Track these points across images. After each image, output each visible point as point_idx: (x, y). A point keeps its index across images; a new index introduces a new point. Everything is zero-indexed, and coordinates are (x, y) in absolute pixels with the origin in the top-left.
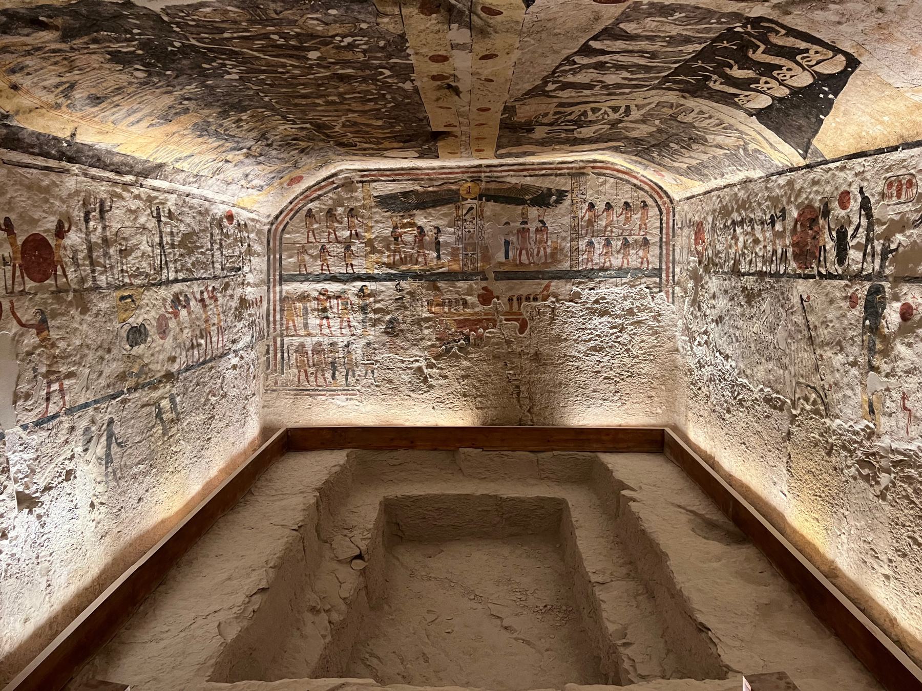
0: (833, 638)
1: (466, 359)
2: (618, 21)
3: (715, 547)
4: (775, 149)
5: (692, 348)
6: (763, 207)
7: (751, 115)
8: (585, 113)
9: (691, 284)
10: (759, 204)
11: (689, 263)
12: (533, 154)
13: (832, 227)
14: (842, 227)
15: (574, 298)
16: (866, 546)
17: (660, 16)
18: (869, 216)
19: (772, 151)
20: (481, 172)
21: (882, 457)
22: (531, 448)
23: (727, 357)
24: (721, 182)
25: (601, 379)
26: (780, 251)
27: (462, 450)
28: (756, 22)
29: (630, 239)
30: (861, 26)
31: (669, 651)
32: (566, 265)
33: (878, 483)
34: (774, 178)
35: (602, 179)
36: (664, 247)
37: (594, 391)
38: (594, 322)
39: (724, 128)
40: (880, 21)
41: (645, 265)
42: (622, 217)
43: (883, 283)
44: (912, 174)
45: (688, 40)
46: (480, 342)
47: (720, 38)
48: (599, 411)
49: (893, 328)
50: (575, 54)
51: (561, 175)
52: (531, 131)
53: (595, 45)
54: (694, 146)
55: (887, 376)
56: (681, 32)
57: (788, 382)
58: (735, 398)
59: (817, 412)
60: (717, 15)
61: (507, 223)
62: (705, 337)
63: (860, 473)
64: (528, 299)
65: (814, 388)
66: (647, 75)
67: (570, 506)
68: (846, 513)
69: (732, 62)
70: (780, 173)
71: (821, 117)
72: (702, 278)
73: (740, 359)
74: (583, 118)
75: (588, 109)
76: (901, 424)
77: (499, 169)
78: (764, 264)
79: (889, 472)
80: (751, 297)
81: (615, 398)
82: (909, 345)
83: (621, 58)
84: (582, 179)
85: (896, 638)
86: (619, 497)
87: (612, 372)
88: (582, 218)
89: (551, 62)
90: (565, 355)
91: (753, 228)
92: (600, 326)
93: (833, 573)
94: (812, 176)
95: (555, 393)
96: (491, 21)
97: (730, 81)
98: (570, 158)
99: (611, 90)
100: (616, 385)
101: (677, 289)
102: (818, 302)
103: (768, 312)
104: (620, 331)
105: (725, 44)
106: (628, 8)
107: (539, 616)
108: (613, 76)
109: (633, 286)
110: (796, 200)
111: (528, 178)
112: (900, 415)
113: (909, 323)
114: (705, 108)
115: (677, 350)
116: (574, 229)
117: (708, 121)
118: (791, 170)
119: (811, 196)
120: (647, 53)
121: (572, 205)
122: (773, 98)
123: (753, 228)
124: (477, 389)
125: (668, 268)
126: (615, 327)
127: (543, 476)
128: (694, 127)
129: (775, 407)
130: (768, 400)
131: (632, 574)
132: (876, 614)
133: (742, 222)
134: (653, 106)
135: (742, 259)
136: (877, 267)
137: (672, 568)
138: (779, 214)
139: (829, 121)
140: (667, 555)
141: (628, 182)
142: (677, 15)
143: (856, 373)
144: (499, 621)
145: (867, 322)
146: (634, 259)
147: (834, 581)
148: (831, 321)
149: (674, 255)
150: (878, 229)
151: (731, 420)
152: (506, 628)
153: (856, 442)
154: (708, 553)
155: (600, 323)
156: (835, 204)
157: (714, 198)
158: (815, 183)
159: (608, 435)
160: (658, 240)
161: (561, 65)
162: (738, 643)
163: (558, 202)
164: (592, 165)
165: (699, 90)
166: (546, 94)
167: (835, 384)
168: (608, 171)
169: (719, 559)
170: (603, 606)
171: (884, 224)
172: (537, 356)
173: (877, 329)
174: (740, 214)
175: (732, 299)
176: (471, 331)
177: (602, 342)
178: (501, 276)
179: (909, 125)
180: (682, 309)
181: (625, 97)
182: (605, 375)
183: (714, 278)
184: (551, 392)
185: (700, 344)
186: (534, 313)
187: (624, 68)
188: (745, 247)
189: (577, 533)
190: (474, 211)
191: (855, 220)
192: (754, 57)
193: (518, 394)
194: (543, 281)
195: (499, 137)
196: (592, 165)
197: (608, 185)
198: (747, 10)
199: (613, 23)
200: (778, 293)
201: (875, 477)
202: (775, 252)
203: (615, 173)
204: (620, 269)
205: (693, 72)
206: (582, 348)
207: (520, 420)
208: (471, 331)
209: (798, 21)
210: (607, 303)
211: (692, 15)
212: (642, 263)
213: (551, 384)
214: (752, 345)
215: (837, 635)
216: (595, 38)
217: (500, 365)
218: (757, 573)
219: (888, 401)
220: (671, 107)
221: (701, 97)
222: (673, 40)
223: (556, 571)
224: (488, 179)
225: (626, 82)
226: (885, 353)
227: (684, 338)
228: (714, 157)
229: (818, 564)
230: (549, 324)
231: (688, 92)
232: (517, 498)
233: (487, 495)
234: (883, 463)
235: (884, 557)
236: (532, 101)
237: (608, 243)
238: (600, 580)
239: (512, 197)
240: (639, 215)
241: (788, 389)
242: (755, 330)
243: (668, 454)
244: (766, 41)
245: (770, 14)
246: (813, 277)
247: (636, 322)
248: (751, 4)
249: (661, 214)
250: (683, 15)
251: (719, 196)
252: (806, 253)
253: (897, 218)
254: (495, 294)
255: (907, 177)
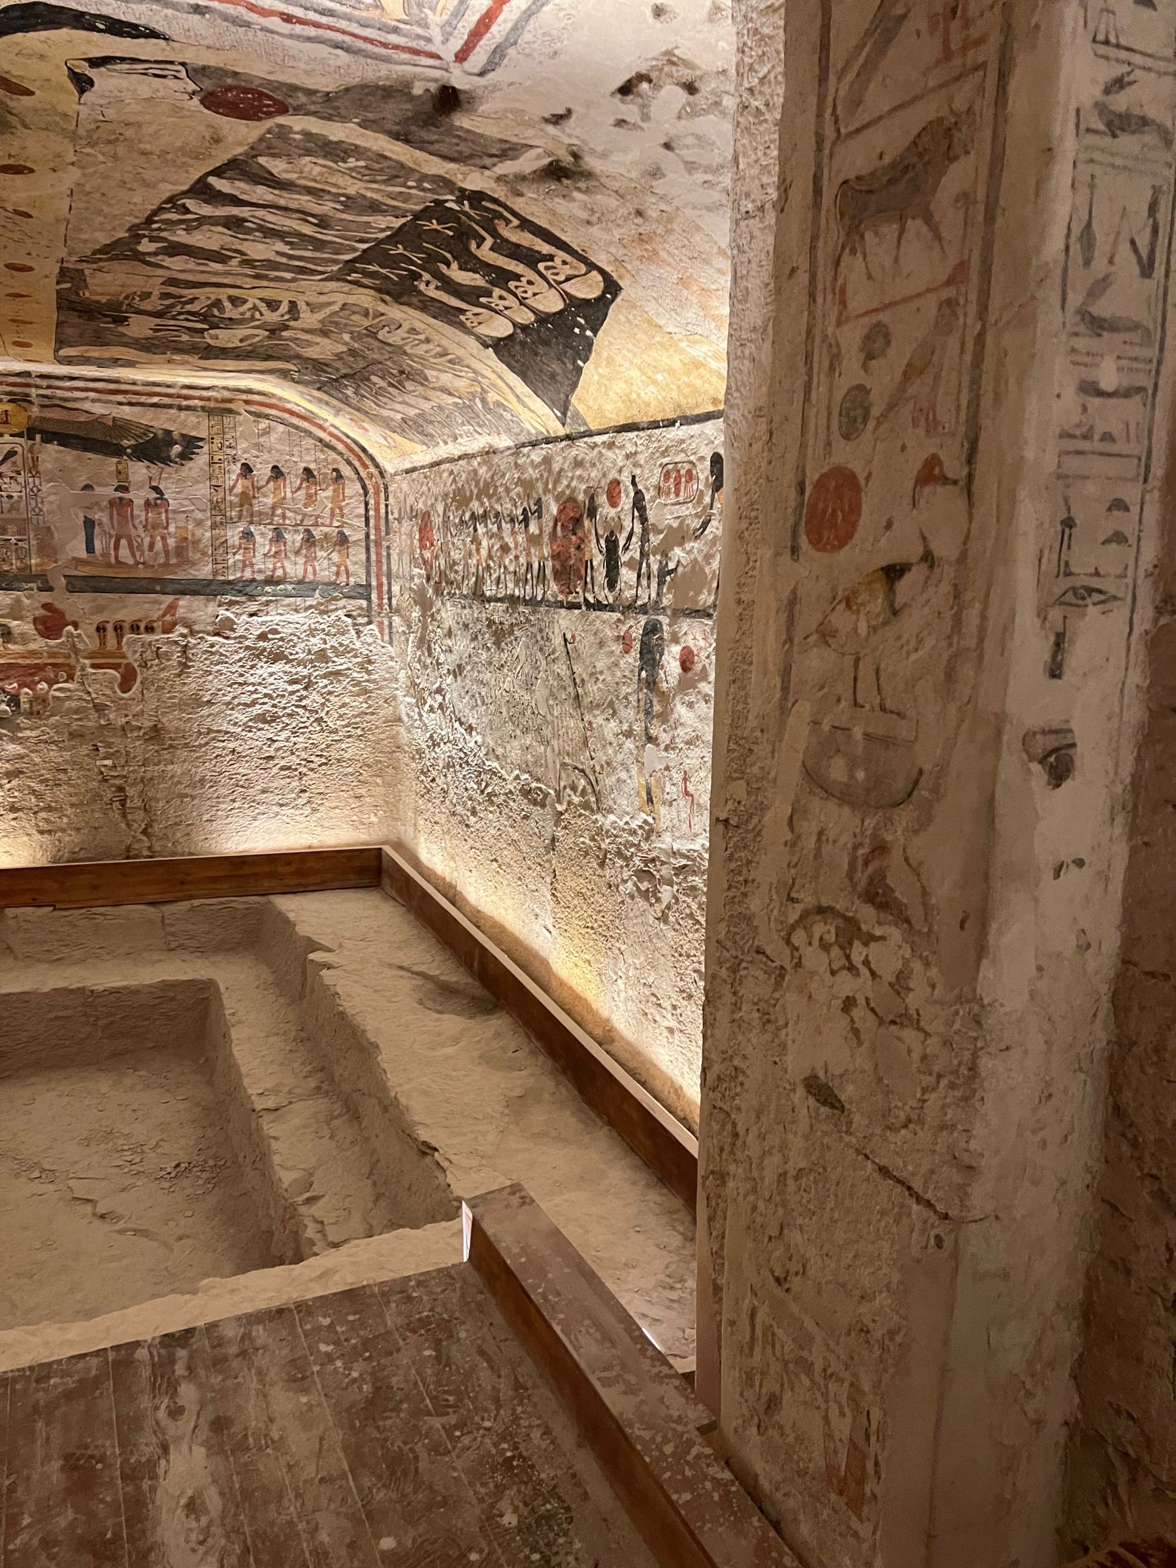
0: (606, 1129)
1: (13, 740)
2: (254, 151)
3: (452, 1023)
4: (524, 405)
5: (420, 715)
6: (513, 494)
7: (486, 346)
8: (218, 303)
9: (416, 614)
10: (508, 490)
11: (412, 578)
12: (131, 364)
13: (600, 532)
14: (612, 533)
15: (223, 629)
16: (647, 992)
17: (325, 157)
18: (643, 519)
19: (520, 408)
20: (28, 385)
21: (663, 863)
22: (151, 898)
23: (470, 729)
24: (453, 450)
25: (275, 770)
26: (536, 566)
27: (10, 912)
28: (477, 198)
29: (317, 533)
30: (617, 233)
31: (378, 1198)
32: (204, 571)
33: (658, 900)
34: (525, 450)
35: (263, 424)
36: (373, 550)
37: (264, 792)
38: (260, 672)
39: (450, 361)
40: (641, 230)
41: (343, 579)
42: (301, 494)
43: (660, 618)
44: (691, 462)
45: (375, 208)
46: (40, 708)
47: (425, 214)
48: (273, 824)
49: (673, 681)
50: (185, 194)
51: (188, 408)
52: (121, 320)
53: (221, 185)
54: (409, 386)
55: (666, 749)
56: (363, 192)
57: (550, 765)
58: (482, 792)
59: (586, 806)
60: (417, 176)
61: (88, 487)
62: (439, 698)
63: (638, 889)
64: (135, 628)
65: (583, 771)
66: (318, 255)
67: (222, 989)
68: (623, 947)
69: (448, 256)
70: (534, 444)
71: (580, 363)
72: (431, 604)
73: (488, 731)
74: (216, 312)
75: (224, 298)
76: (684, 815)
77: (68, 384)
78: (517, 585)
79: (670, 883)
80: (500, 634)
81: (301, 801)
82: (690, 705)
83: (270, 217)
84: (228, 420)
85: (681, 1114)
86: (304, 963)
87: (294, 758)
88: (231, 489)
89: (143, 201)
90: (210, 731)
91: (499, 528)
92: (271, 680)
93: (607, 1038)
94: (574, 452)
95: (193, 798)
96: (12, 104)
97: (448, 285)
98: (204, 379)
99: (261, 270)
100: (301, 779)
101: (396, 620)
102: (585, 645)
103: (523, 658)
104: (306, 688)
105: (435, 225)
106: (269, 131)
107: (166, 1185)
108: (261, 247)
109: (326, 612)
110: (554, 488)
111: (127, 408)
112: (682, 803)
113: (690, 674)
114: (418, 325)
115: (400, 720)
116: (216, 507)
117: (425, 347)
118: (548, 441)
119: (574, 484)
120: (313, 216)
121: (211, 463)
122: (515, 325)
123: (499, 528)
124: (39, 796)
125: (380, 585)
126: (295, 682)
127: (173, 947)
128: (405, 353)
129: (535, 803)
130: (526, 792)
131: (325, 1087)
132: (658, 1085)
133: (485, 515)
134: (336, 308)
135: (486, 576)
136: (654, 595)
137: (384, 1065)
138: (534, 508)
139: (591, 371)
140: (377, 1047)
141: (309, 434)
142: (352, 162)
143: (632, 746)
144: (88, 1208)
145: (644, 674)
146: (324, 566)
147: (610, 1048)
148: (601, 673)
149: (389, 563)
150: (655, 540)
151: (478, 826)
152: (102, 1217)
153: (633, 845)
154: (439, 1034)
155: (271, 674)
156: (603, 499)
157: (445, 475)
158: (578, 464)
159: (289, 864)
160: (362, 536)
161: (160, 210)
162: (475, 1162)
163: (185, 456)
164: (244, 397)
165: (402, 291)
166: (139, 257)
167: (608, 764)
168: (274, 412)
169: (455, 1041)
170: (275, 1145)
171: (661, 532)
172: (156, 734)
173: (655, 683)
174: (482, 504)
175: (474, 638)
176: (21, 686)
177: (274, 706)
178: (76, 585)
179: (686, 390)
180: (404, 652)
181: (287, 285)
182: (283, 763)
183: (448, 604)
184: (186, 796)
185: (432, 710)
186: (148, 655)
187: (280, 235)
188: (490, 557)
189: (234, 1034)
190: (18, 458)
191: (627, 524)
192: (478, 253)
193: (123, 803)
194: (163, 597)
195: (59, 324)
196: (244, 397)
197: (274, 437)
198: (460, 177)
199: (246, 154)
200: (534, 630)
201: (656, 892)
202: (529, 566)
203: (286, 416)
204: (301, 582)
205: (393, 262)
206: (241, 717)
207: (129, 848)
208: (21, 686)
209: (534, 209)
210: (282, 639)
211: (377, 166)
212: (338, 574)
213: (186, 780)
214: (504, 710)
215: (610, 1123)
216: (218, 172)
217: (84, 749)
218: (510, 1054)
219: (668, 784)
220: (366, 314)
221: (409, 305)
222: (350, 203)
223: (198, 1105)
224: (46, 402)
225: (284, 260)
226: (664, 717)
227: (408, 699)
228: (440, 407)
229: (590, 1027)
230: (179, 675)
231: (388, 294)
232: (124, 988)
233: (65, 989)
234: (666, 871)
235: (666, 1004)
236: (115, 265)
237: (278, 537)
238: (271, 1103)
239: (98, 439)
240: (329, 493)
241: (551, 775)
242: (506, 686)
243: (388, 888)
244: (495, 234)
245: (492, 190)
246: (578, 606)
247: (331, 673)
248: (465, 169)
249: (366, 494)
250: (362, 163)
251: (452, 473)
252: (568, 571)
253: (675, 524)
254: (68, 618)
255: (687, 466)
